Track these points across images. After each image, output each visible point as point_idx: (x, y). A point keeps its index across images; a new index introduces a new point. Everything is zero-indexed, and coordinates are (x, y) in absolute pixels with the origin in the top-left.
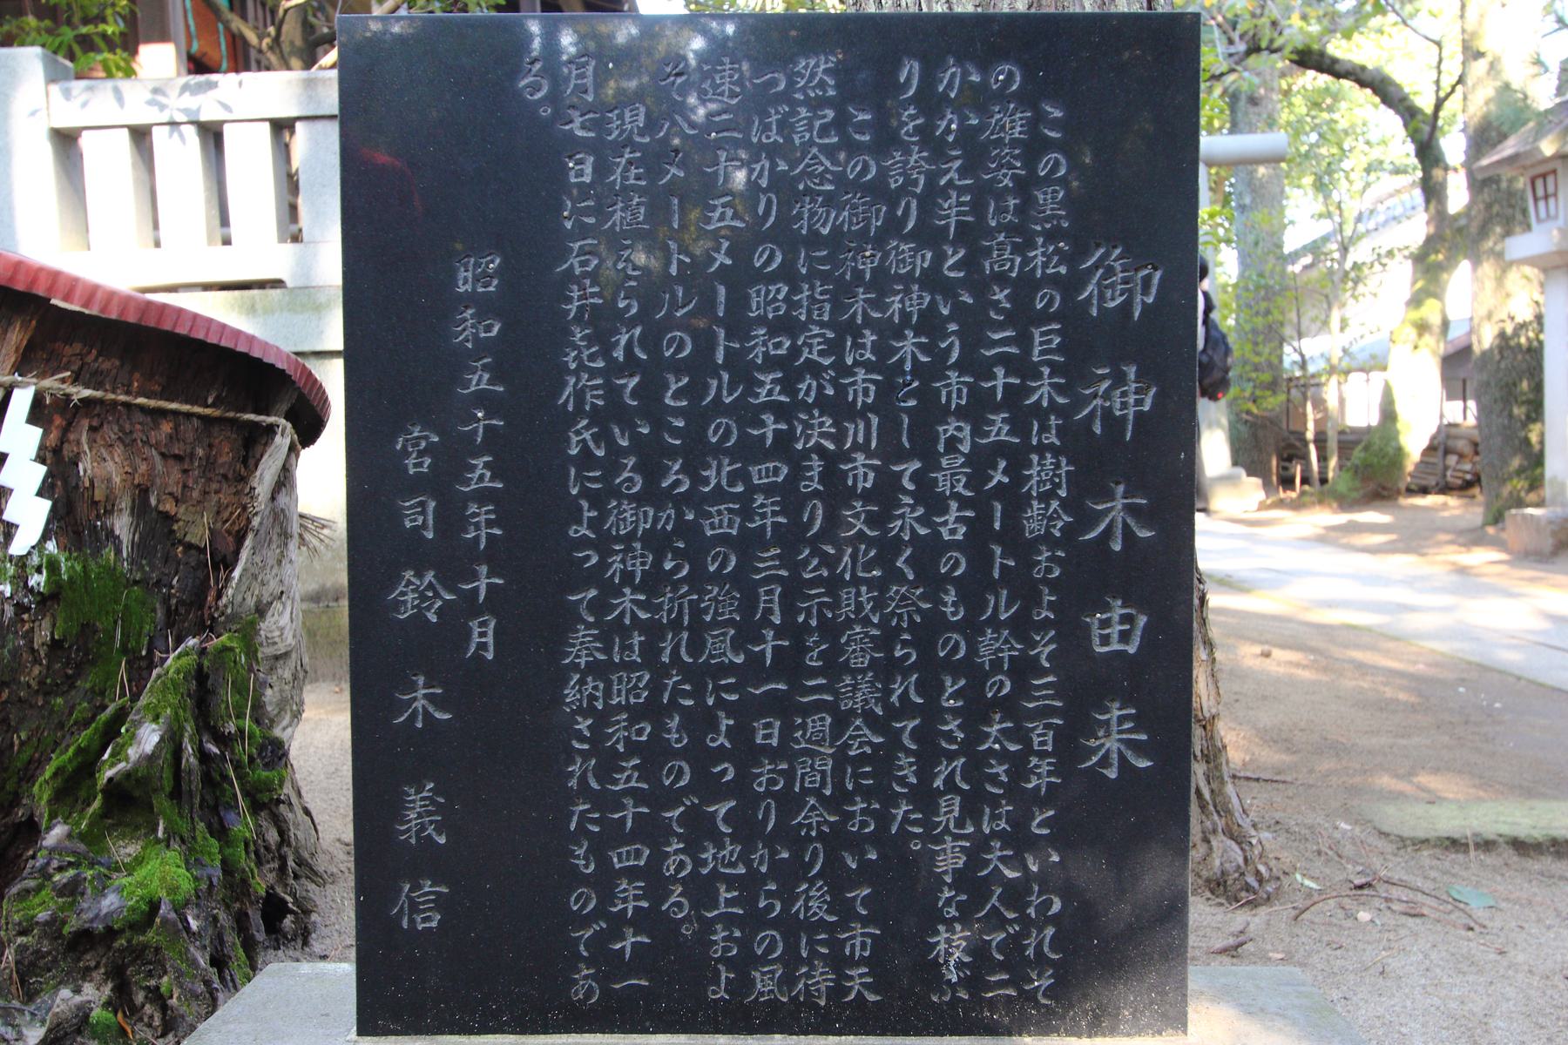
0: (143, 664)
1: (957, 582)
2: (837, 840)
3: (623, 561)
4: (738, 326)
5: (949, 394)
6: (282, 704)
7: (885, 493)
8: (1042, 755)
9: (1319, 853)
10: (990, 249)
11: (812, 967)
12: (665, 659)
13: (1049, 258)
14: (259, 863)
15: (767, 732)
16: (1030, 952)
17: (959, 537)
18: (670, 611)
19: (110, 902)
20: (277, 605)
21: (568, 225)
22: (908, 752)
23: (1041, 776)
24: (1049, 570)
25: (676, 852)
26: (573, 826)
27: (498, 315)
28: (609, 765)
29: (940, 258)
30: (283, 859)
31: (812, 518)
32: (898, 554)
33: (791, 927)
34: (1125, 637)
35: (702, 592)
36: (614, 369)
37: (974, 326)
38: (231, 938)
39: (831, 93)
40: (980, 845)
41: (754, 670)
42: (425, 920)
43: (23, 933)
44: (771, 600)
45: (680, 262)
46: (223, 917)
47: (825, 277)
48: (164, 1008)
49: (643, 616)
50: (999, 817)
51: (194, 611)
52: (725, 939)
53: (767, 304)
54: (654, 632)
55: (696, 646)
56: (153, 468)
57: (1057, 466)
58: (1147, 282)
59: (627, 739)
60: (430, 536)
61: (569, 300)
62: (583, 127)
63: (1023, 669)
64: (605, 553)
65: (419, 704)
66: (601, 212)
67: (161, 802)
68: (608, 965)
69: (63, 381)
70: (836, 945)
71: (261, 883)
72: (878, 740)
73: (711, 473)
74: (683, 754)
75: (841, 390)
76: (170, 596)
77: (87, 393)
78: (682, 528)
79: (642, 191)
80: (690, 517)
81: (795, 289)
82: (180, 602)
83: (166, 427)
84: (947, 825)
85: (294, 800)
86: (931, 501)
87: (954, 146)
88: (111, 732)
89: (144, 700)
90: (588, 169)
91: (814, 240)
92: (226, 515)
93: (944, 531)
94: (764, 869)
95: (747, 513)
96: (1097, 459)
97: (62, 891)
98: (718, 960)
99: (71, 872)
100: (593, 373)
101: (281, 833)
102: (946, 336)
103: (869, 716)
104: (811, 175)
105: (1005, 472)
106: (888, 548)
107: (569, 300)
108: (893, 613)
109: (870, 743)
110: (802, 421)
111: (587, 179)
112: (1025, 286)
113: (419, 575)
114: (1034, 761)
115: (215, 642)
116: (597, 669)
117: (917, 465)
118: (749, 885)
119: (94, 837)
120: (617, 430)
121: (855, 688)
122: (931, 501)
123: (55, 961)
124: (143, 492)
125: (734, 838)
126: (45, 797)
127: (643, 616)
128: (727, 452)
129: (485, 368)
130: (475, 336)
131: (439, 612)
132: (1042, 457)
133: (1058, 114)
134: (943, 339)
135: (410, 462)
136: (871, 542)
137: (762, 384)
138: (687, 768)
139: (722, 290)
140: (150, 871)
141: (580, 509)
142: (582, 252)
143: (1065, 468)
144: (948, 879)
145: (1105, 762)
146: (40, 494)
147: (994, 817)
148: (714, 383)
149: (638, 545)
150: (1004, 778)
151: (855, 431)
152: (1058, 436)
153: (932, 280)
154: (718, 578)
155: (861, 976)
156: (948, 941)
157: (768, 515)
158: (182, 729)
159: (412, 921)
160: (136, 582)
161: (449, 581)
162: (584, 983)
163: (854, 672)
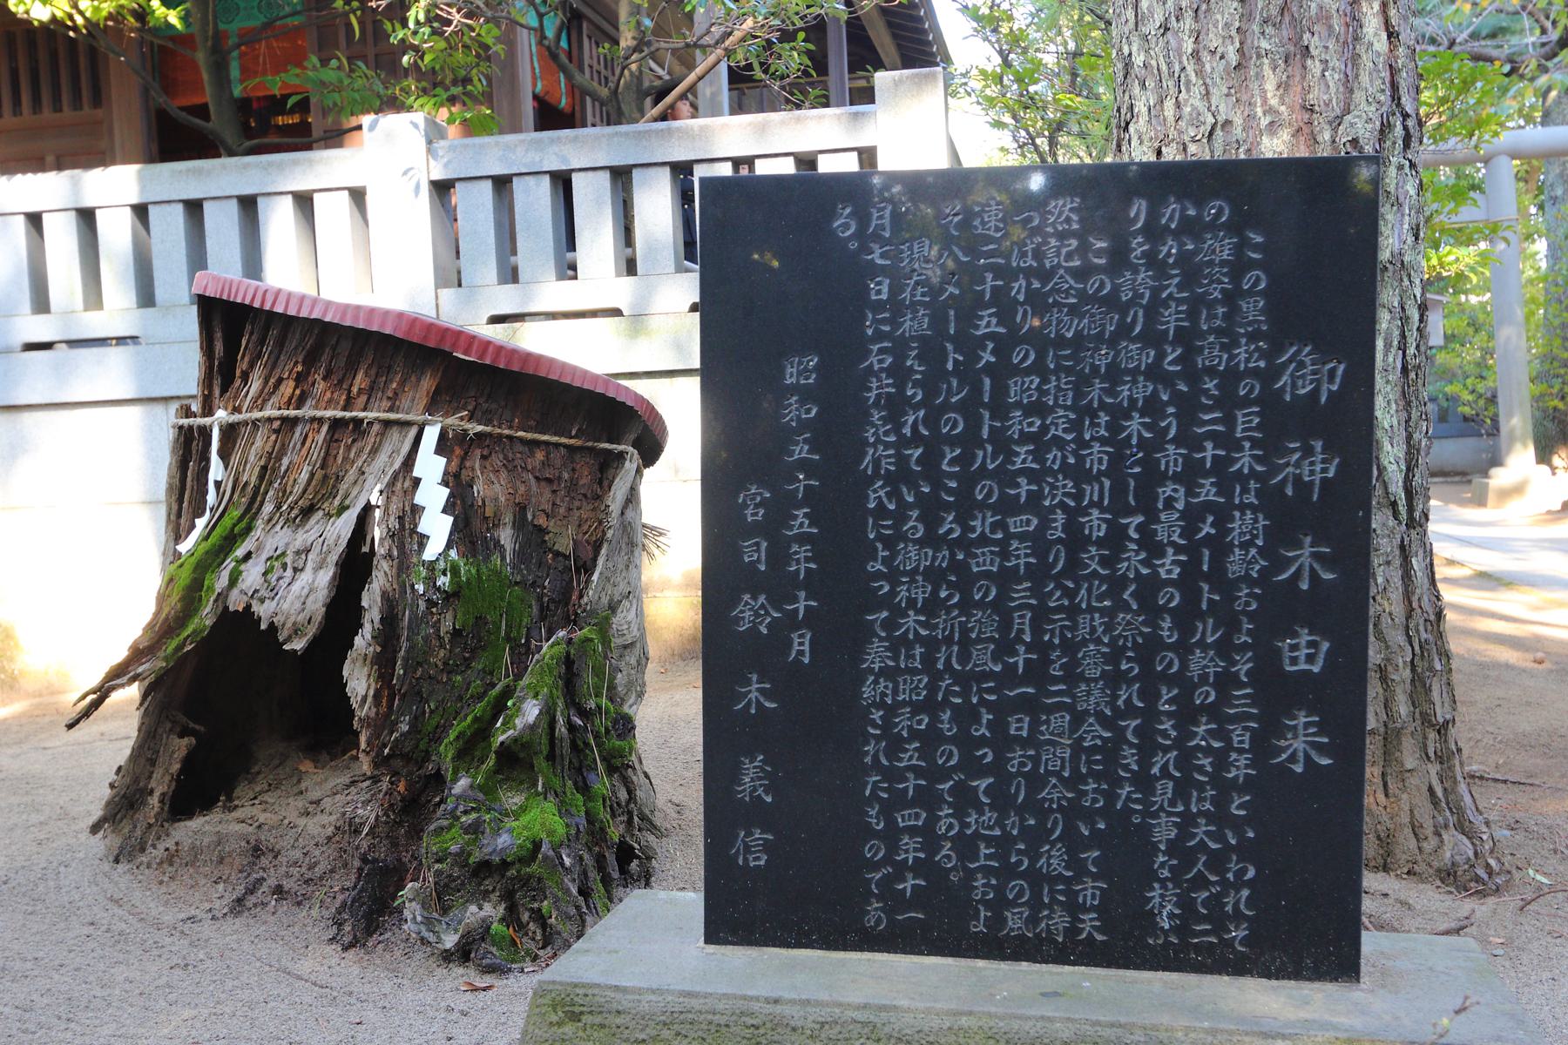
0: (523, 650)
1: (1171, 611)
2: (1073, 812)
3: (908, 590)
4: (1000, 409)
5: (1167, 463)
6: (630, 685)
7: (1115, 539)
8: (1241, 751)
9: (1555, 851)
10: (1202, 348)
11: (1052, 911)
12: (940, 666)
13: (1251, 354)
14: (613, 816)
15: (1019, 726)
16: (1229, 908)
17: (1174, 576)
18: (944, 630)
19: (503, 840)
20: (625, 603)
21: (870, 332)
22: (1131, 745)
23: (1240, 768)
24: (1247, 604)
25: (947, 816)
26: (867, 793)
27: (815, 402)
28: (895, 746)
29: (1161, 356)
30: (630, 814)
31: (1056, 559)
32: (1125, 588)
33: (1036, 878)
34: (1310, 659)
35: (969, 615)
36: (903, 442)
37: (1188, 408)
38: (594, 875)
39: (1075, 226)
40: (1188, 820)
41: (1009, 676)
42: (756, 859)
43: (438, 861)
44: (1023, 622)
45: (955, 360)
46: (586, 856)
47: (1069, 371)
48: (544, 925)
49: (924, 632)
50: (1205, 799)
51: (562, 607)
52: (984, 885)
53: (1023, 392)
54: (931, 645)
55: (964, 657)
56: (529, 490)
57: (1256, 521)
58: (1332, 374)
59: (910, 727)
60: (763, 568)
61: (870, 389)
62: (882, 256)
63: (1225, 682)
64: (895, 583)
65: (753, 696)
66: (894, 322)
67: (540, 763)
68: (894, 902)
69: (462, 419)
70: (1070, 893)
71: (615, 832)
72: (1107, 735)
73: (977, 523)
74: (951, 740)
75: (1081, 459)
76: (543, 595)
77: (480, 428)
78: (955, 566)
79: (925, 305)
80: (961, 557)
81: (1045, 381)
82: (551, 600)
83: (540, 455)
84: (1162, 806)
85: (637, 766)
86: (1152, 547)
87: (1173, 267)
88: (499, 707)
89: (526, 681)
90: (885, 289)
91: (1060, 342)
92: (585, 528)
93: (1162, 571)
94: (1015, 832)
95: (1005, 554)
96: (1288, 516)
97: (467, 829)
98: (978, 902)
99: (474, 815)
100: (887, 446)
101: (630, 792)
102: (1166, 416)
103: (1100, 716)
104: (1059, 291)
105: (1213, 525)
106: (1117, 584)
107: (870, 389)
108: (1120, 636)
109: (1100, 737)
110: (1049, 484)
111: (884, 297)
112: (1231, 377)
113: (755, 598)
114: (1234, 756)
115: (579, 634)
116: (887, 673)
117: (1140, 519)
118: (1003, 844)
119: (488, 789)
120: (905, 489)
121: (1089, 693)
122: (1152, 547)
123: (463, 884)
124: (521, 509)
125: (992, 807)
126: (450, 756)
127: (924, 632)
128: (989, 507)
129: (805, 441)
130: (799, 417)
131: (769, 626)
132: (1243, 514)
133: (1259, 239)
134: (1163, 419)
135: (749, 512)
136: (1102, 579)
137: (1018, 454)
138: (955, 751)
139: (987, 381)
140: (532, 819)
141: (876, 549)
142: (881, 351)
143: (1262, 523)
144: (1163, 847)
145: (1293, 758)
146: (444, 511)
147: (1200, 800)
148: (980, 453)
149: (920, 578)
150: (1209, 769)
151: (1091, 492)
152: (1256, 497)
153: (1154, 373)
154: (981, 604)
155: (1091, 920)
156: (1162, 896)
157: (1022, 556)
158: (555, 704)
159: (746, 859)
160: (517, 583)
161: (776, 602)
162: (875, 914)
163: (1088, 681)
